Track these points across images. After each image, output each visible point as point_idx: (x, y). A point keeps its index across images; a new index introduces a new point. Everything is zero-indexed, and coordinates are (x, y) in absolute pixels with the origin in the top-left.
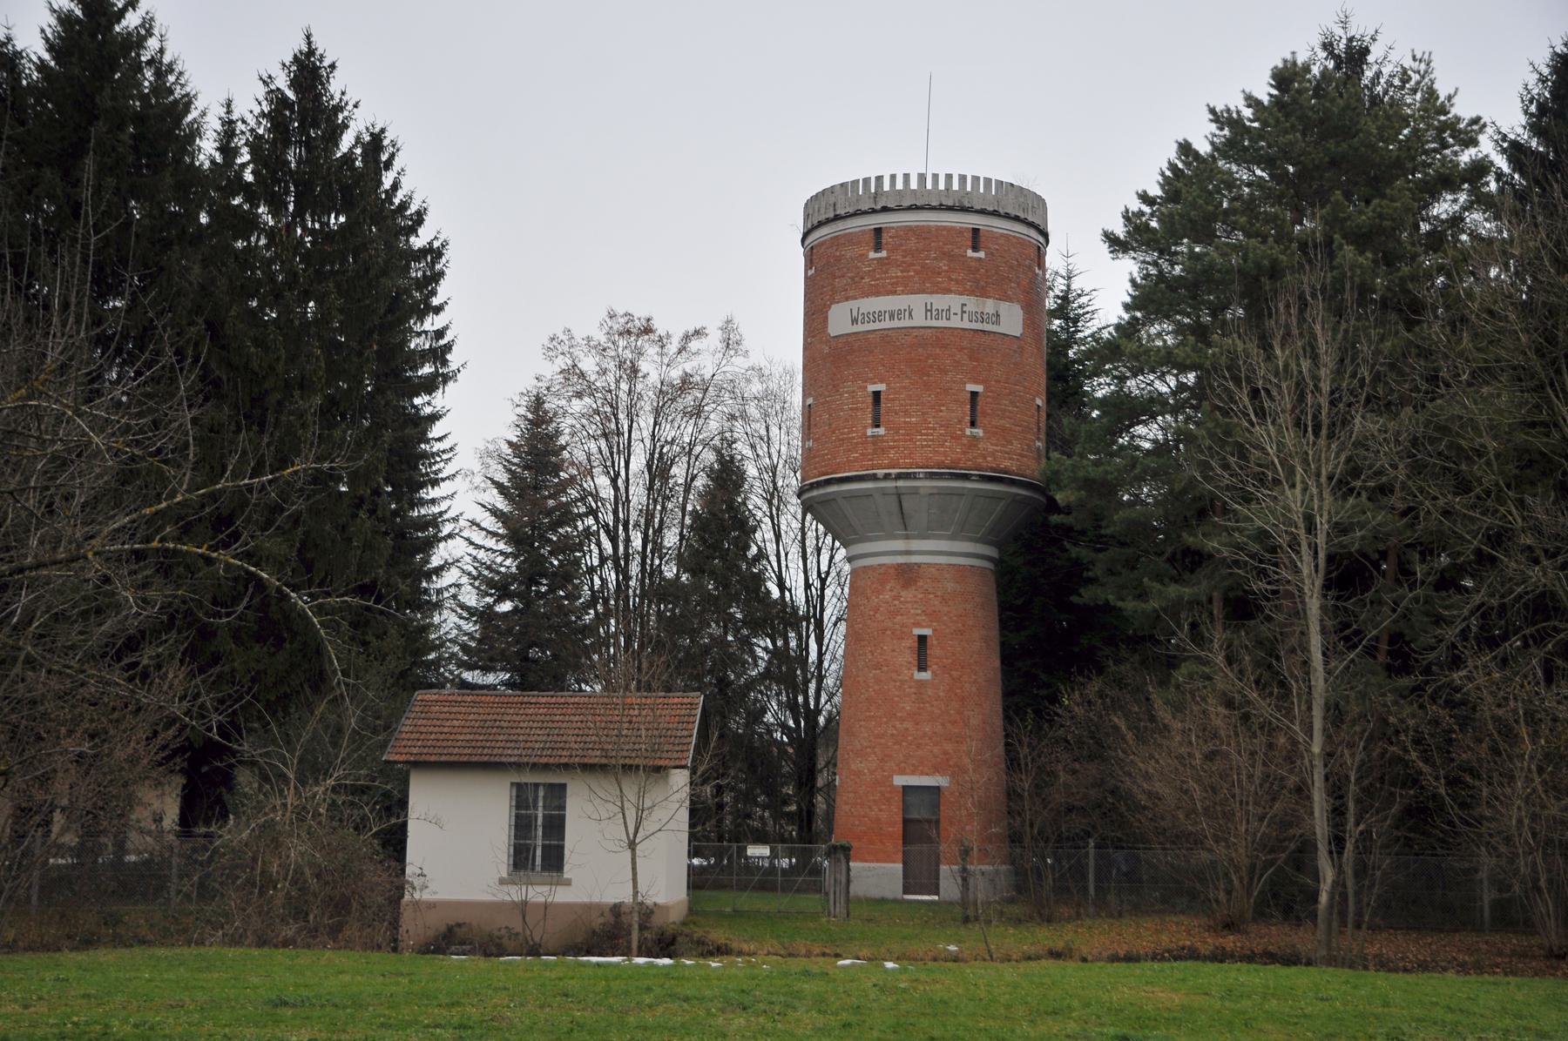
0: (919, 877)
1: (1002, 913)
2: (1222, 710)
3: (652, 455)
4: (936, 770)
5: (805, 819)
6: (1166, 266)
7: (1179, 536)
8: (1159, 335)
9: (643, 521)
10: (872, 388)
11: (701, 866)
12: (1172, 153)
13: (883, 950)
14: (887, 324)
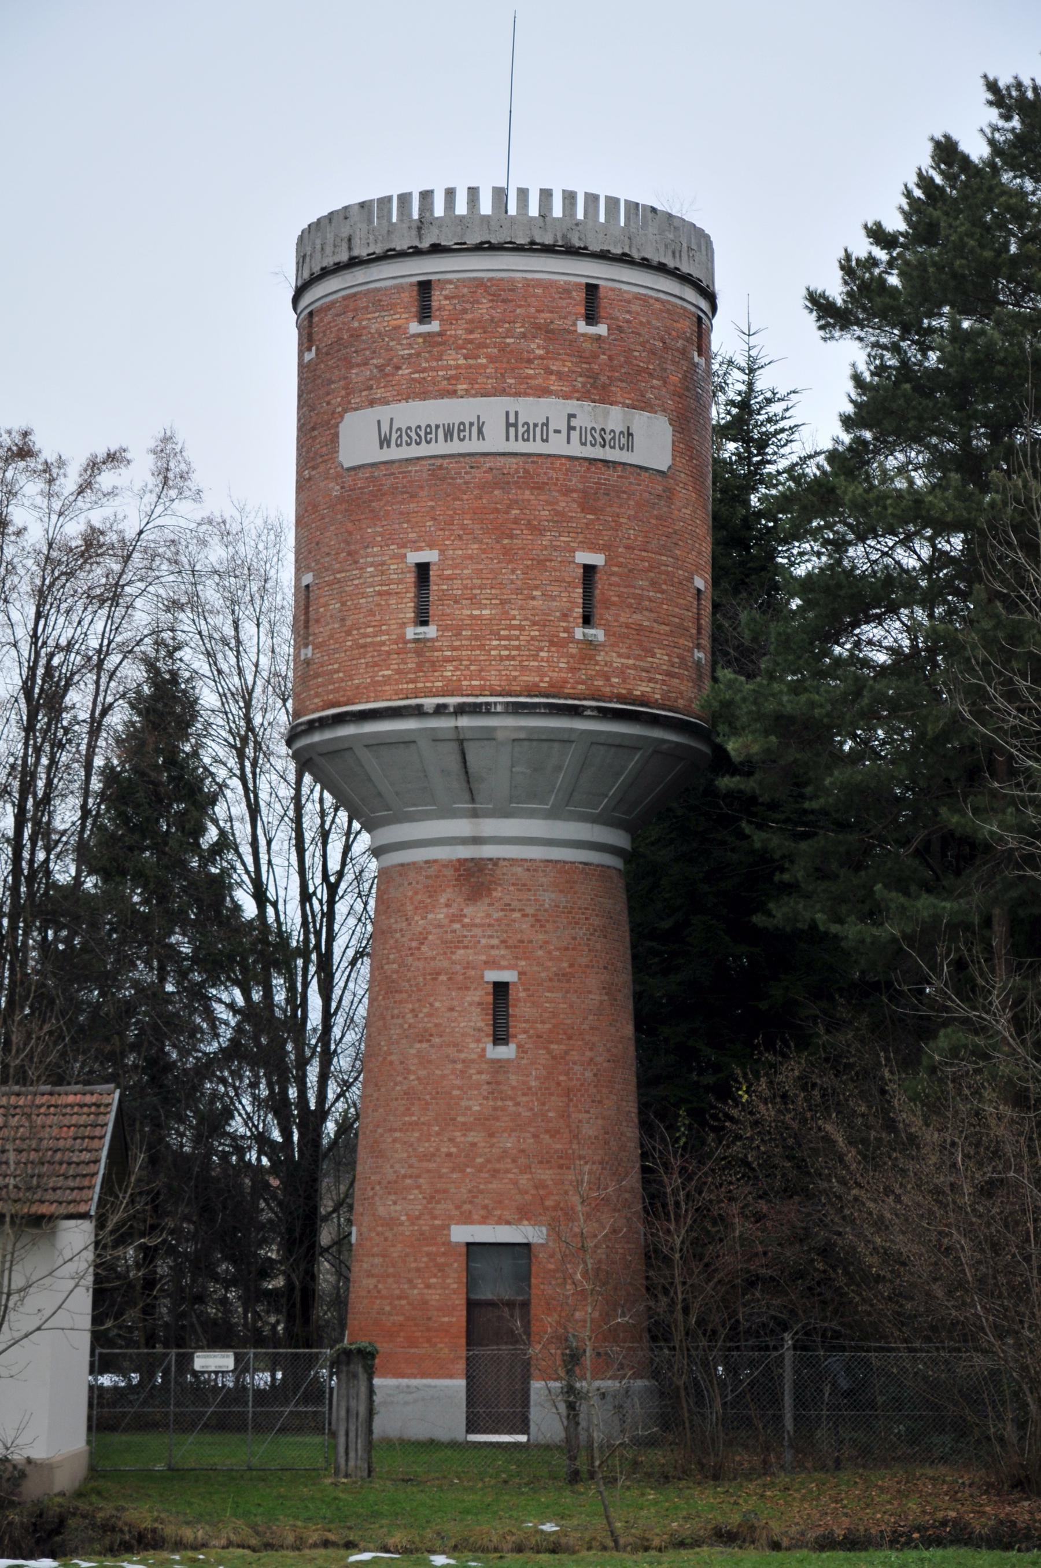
0: (494, 1401)
1: (636, 1464)
2: (1007, 1111)
3: (33, 669)
4: (524, 1214)
5: (300, 1301)
6: (913, 353)
7: (936, 814)
8: (902, 470)
9: (16, 784)
10: (415, 557)
11: (115, 1388)
12: (924, 158)
13: (429, 1534)
14: (440, 447)
